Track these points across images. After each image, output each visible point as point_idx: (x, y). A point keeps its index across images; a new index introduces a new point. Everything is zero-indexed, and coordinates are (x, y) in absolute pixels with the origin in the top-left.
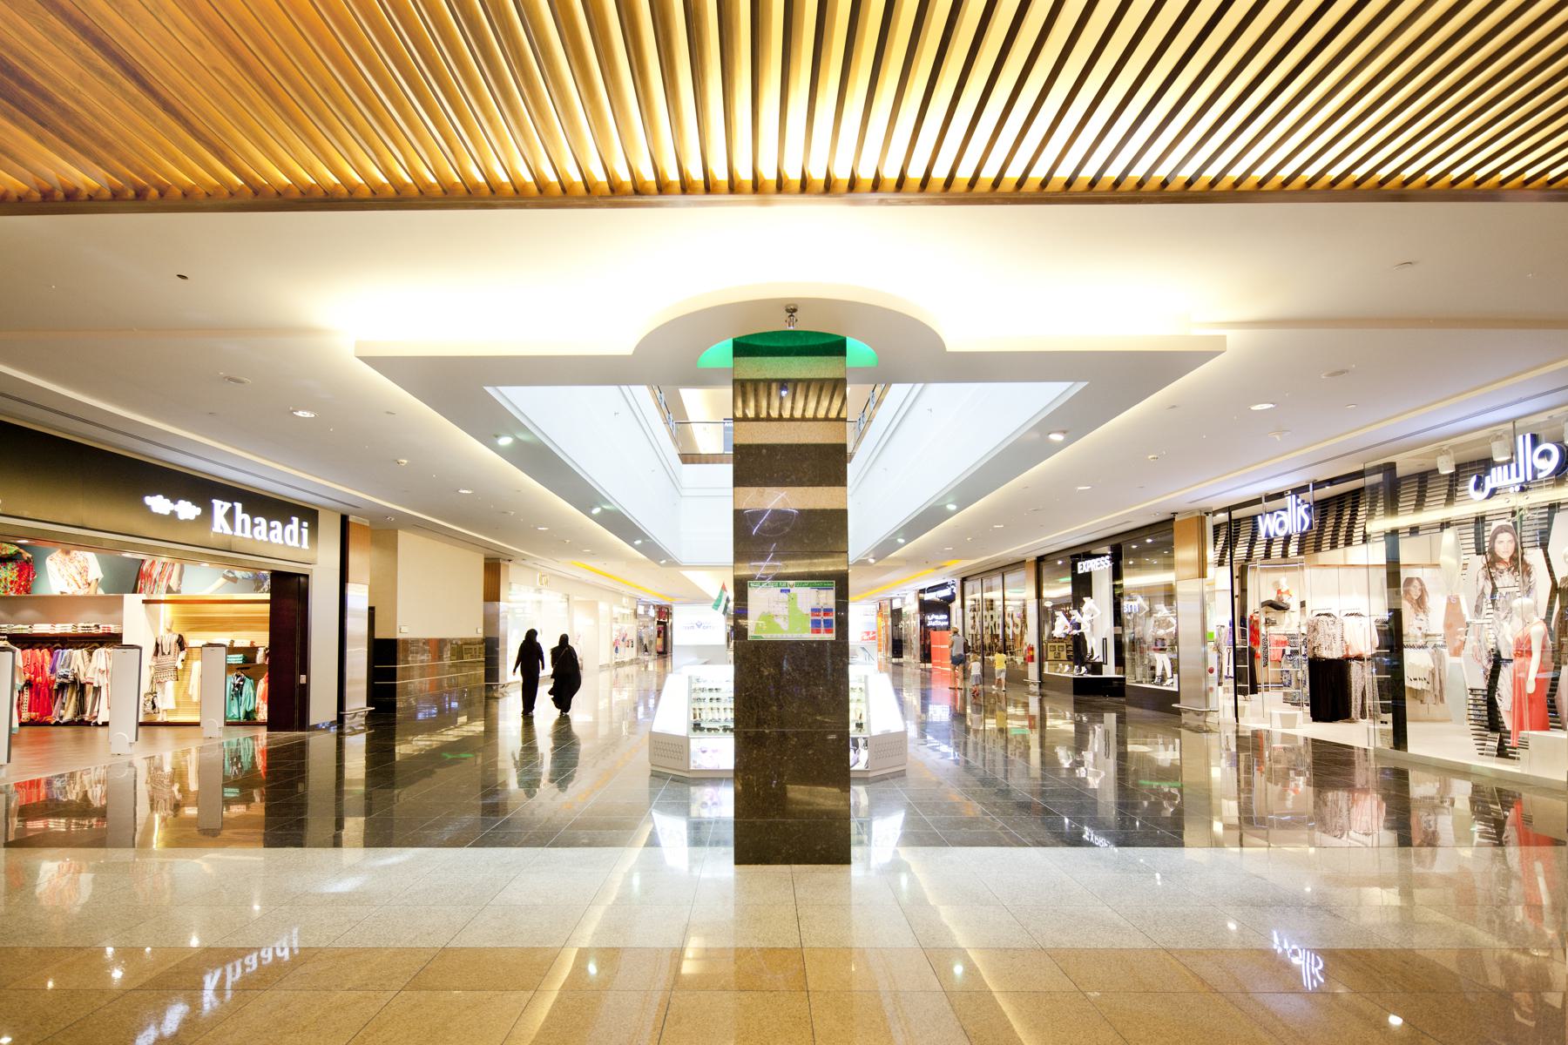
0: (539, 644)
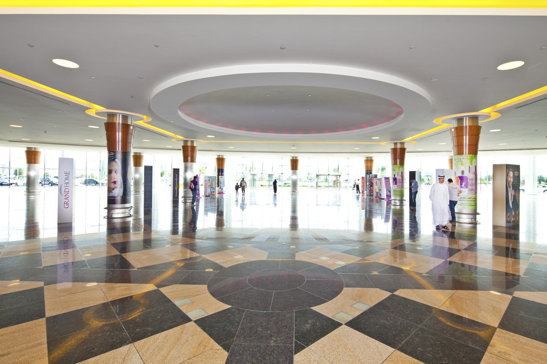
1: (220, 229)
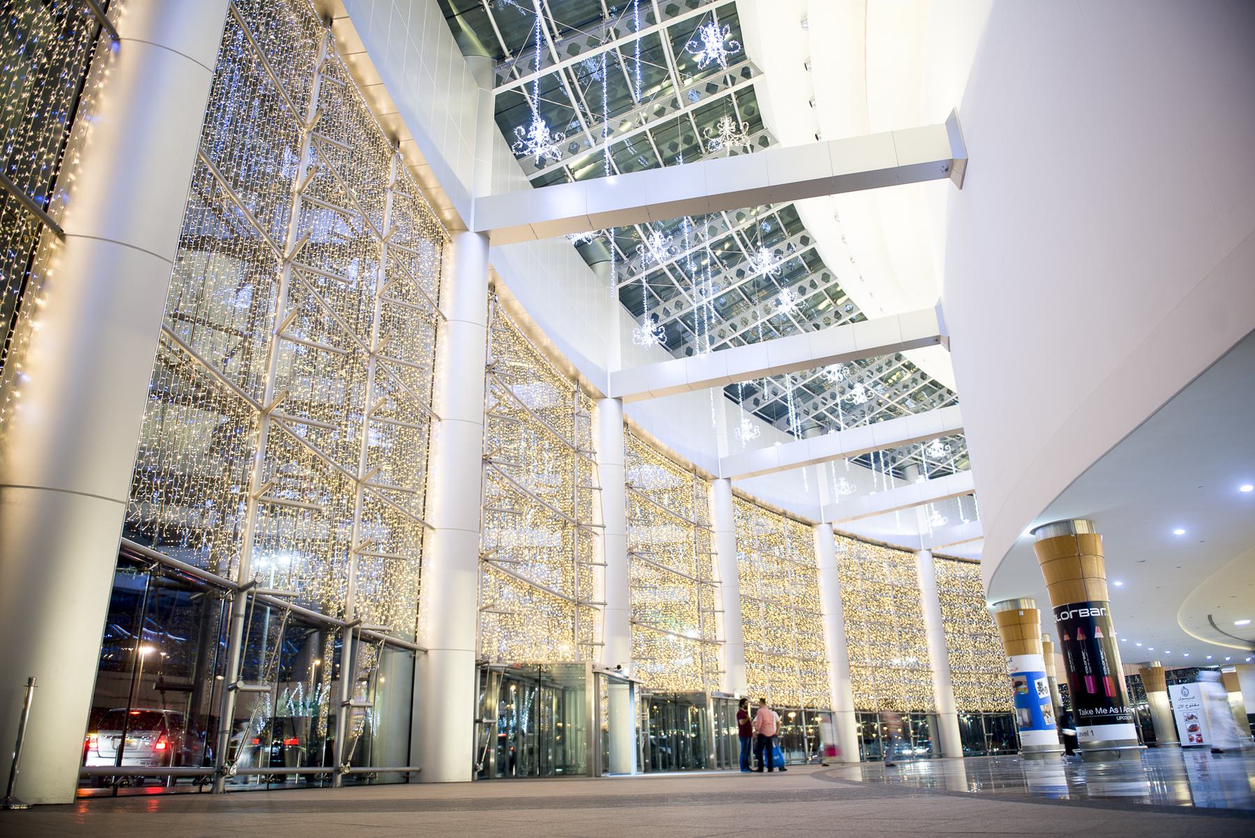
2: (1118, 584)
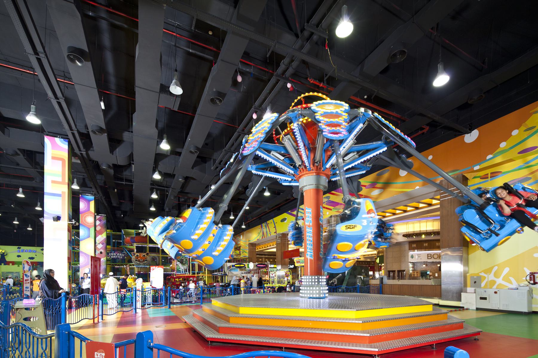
0: (56, 281)
1: (311, 251)
2: (366, 97)
